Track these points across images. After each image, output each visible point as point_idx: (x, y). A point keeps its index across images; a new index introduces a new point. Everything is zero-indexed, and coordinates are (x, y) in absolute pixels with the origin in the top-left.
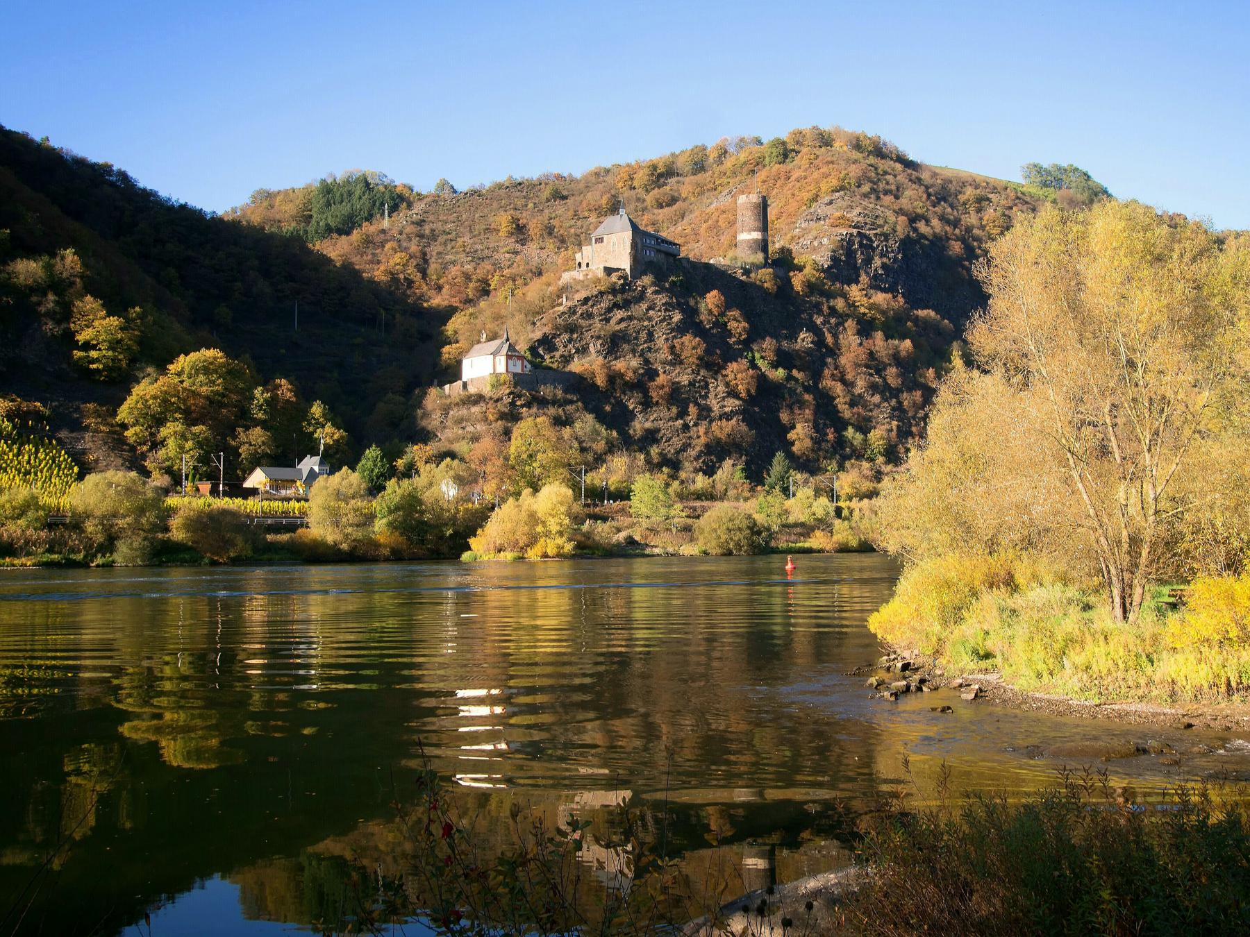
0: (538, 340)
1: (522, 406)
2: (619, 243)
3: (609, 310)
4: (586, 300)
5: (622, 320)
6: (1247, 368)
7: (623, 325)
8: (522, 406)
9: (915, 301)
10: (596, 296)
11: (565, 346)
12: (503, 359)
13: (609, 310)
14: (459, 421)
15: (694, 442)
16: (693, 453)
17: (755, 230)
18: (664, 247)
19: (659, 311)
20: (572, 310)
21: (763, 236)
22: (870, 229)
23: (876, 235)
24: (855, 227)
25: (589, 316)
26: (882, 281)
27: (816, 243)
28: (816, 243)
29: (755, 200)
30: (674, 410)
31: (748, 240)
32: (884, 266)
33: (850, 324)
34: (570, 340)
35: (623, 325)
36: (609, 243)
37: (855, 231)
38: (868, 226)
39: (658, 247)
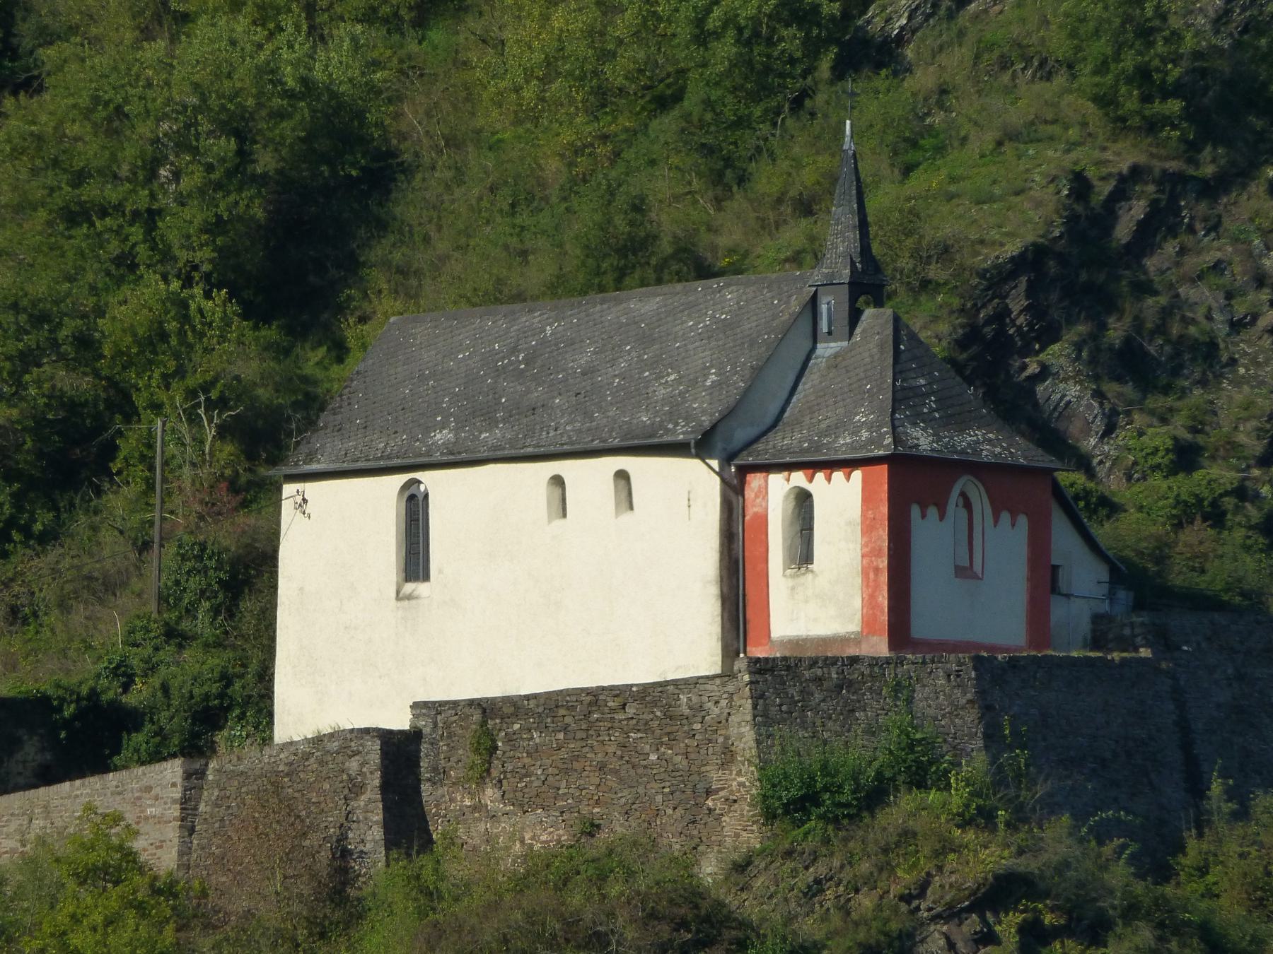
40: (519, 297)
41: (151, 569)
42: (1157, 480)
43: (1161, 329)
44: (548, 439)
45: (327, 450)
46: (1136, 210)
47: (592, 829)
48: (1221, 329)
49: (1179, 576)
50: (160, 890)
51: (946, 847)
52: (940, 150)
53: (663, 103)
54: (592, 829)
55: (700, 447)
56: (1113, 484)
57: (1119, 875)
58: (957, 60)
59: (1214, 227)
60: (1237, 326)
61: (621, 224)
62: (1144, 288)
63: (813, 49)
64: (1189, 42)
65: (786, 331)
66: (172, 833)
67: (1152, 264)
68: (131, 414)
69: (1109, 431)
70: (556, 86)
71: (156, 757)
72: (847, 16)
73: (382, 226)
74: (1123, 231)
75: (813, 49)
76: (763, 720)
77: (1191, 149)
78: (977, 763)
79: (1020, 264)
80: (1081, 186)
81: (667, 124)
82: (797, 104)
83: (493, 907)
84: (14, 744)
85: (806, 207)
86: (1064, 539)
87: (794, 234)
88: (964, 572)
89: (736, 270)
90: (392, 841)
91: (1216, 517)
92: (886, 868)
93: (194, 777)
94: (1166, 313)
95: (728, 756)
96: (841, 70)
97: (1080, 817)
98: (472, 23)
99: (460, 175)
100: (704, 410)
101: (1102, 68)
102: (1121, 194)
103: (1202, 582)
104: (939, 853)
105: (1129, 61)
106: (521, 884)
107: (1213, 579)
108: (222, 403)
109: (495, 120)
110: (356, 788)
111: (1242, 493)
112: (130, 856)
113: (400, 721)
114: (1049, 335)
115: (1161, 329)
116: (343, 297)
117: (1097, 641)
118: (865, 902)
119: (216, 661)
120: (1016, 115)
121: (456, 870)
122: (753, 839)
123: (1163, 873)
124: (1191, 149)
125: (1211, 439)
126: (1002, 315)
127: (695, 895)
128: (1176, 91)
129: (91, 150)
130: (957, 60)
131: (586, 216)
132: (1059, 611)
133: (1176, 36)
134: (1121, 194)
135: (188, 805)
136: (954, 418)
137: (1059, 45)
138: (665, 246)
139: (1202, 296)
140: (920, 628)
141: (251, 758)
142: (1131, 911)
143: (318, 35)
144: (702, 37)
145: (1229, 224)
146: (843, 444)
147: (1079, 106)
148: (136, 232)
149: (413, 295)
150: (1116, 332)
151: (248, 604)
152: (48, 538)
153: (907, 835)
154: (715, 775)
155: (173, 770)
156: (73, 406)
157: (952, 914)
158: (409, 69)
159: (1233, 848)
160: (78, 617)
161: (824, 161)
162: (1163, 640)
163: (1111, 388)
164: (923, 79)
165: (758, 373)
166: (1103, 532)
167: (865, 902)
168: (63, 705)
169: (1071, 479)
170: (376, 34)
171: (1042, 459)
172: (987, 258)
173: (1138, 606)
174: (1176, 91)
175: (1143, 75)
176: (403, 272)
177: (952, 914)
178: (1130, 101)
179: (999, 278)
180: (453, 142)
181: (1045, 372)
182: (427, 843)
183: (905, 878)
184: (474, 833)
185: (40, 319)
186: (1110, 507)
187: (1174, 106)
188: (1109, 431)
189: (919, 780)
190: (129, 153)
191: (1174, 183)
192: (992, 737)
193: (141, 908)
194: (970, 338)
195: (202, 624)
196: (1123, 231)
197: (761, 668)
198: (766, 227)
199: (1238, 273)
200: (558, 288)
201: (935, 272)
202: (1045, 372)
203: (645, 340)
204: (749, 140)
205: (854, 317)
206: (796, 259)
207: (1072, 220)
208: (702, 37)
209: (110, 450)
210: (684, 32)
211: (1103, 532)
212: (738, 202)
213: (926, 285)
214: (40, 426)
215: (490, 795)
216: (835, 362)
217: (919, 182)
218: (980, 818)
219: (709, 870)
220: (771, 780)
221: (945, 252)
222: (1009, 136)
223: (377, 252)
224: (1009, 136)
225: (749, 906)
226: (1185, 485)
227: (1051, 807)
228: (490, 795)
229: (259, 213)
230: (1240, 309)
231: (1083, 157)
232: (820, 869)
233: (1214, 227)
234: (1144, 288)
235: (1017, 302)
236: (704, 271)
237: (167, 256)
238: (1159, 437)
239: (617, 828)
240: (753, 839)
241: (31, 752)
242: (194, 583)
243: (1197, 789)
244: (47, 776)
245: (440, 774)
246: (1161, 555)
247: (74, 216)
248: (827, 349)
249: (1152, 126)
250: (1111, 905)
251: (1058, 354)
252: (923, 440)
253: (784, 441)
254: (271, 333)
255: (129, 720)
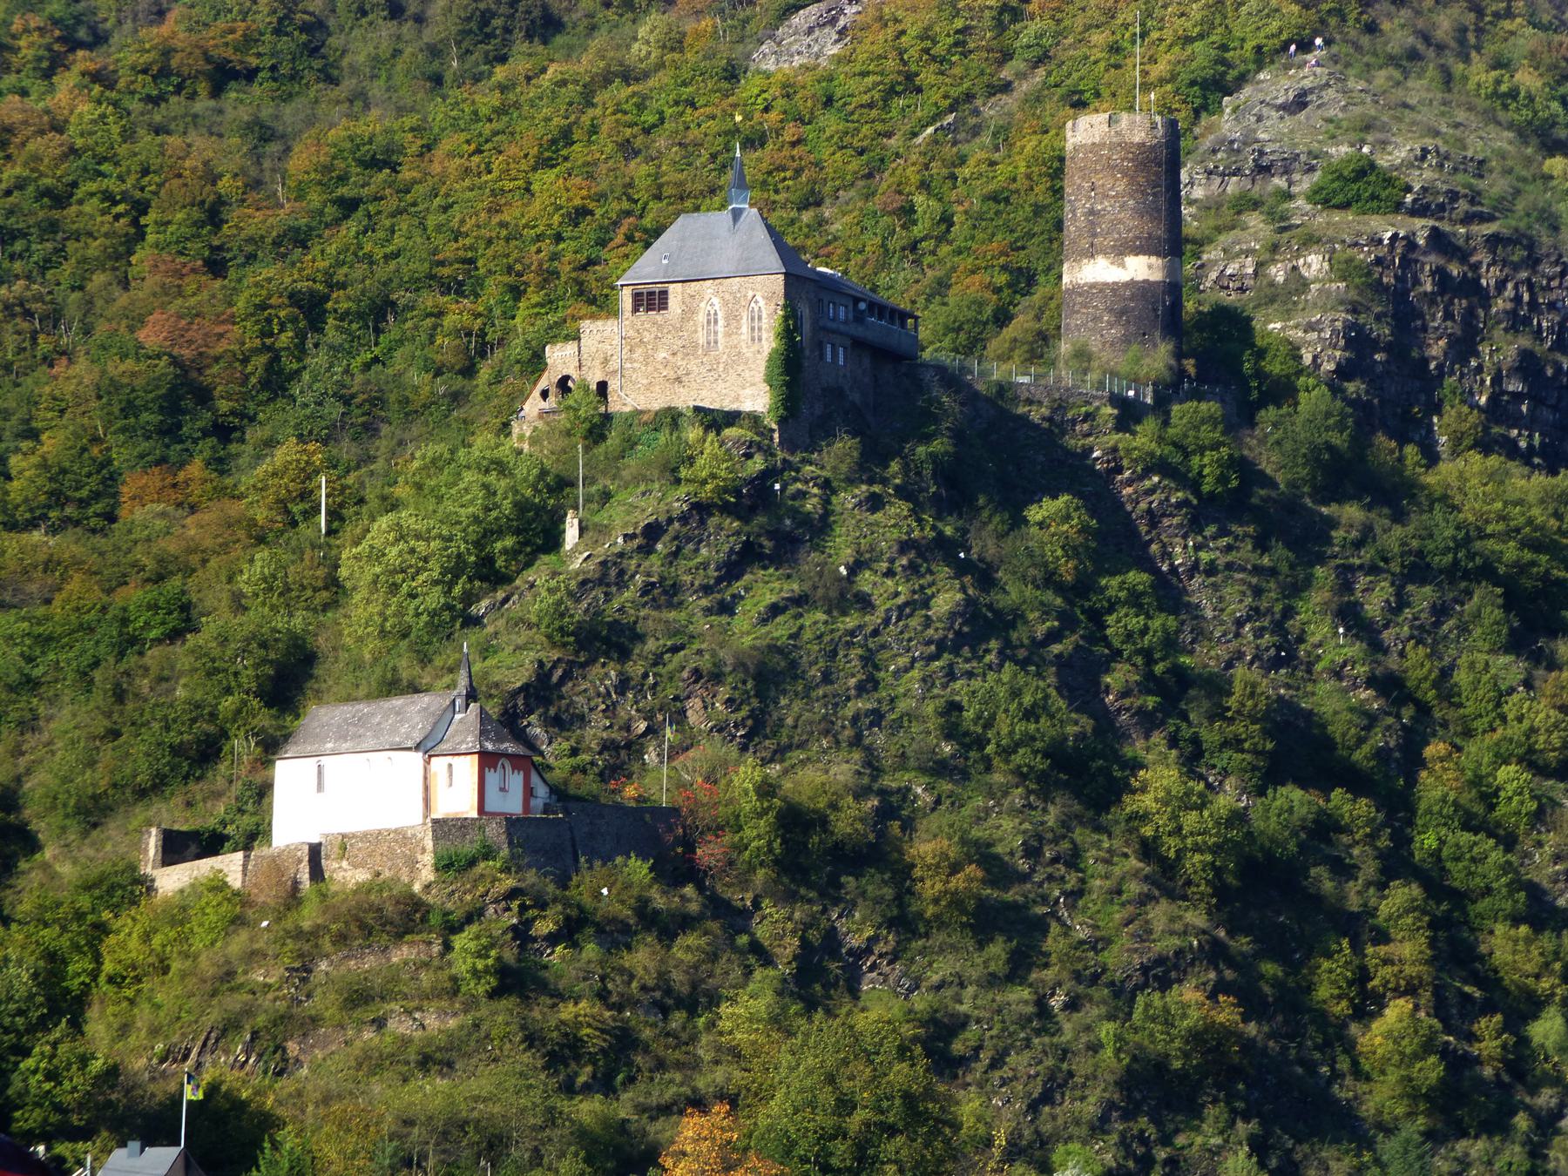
0: (525, 688)
1: (553, 939)
2: (732, 318)
3: (733, 569)
4: (653, 532)
5: (775, 610)
6: (263, 17)
7: (780, 629)
8: (553, 939)
9: (1200, 532)
10: (684, 519)
11: (610, 711)
12: (467, 768)
13: (733, 569)
14: (358, 998)
15: (1081, 1066)
16: (1090, 1108)
17: (1138, 251)
18: (875, 328)
19: (890, 573)
20: (610, 575)
21: (1173, 270)
22: (1468, 219)
23: (1494, 241)
24: (1419, 210)
25: (665, 593)
26: (1516, 421)
27: (1278, 273)
28: (1278, 273)
29: (1139, 136)
30: (998, 949)
31: (1115, 288)
32: (1528, 365)
33: (1484, 603)
34: (623, 685)
35: (780, 629)
36: (689, 313)
37: (1421, 228)
38: (1463, 206)
39: (859, 331)
40: (356, 699)
41: (233, 788)
42: (565, 760)
43: (567, 710)
44: (365, 746)
45: (291, 750)
46: (559, 672)
47: (378, 874)
48: (586, 710)
49: (572, 791)
50: (236, 894)
51: (494, 880)
52: (495, 652)
53: (405, 636)
54: (378, 874)
55: (417, 748)
56: (551, 761)
57: (551, 888)
58: (501, 623)
59: (584, 678)
60: (591, 710)
61: (389, 675)
62: (562, 697)
63: (453, 619)
64: (577, 618)
65: (445, 710)
66: (239, 876)
67: (564, 689)
68: (228, 738)
69: (550, 743)
70: (370, 629)
71: (235, 850)
72: (465, 609)
73: (311, 676)
74: (555, 679)
75: (453, 619)
76: (436, 838)
77: (577, 653)
78: (505, 852)
79: (521, 689)
80: (541, 664)
81: (404, 644)
82: (448, 637)
83: (344, 900)
84: (188, 847)
85: (451, 670)
86: (535, 779)
87: (447, 679)
88: (503, 789)
89: (426, 691)
90: (312, 878)
91: (584, 771)
92: (475, 887)
93: (247, 857)
94: (568, 705)
95: (424, 851)
96: (462, 627)
97: (539, 869)
98: (342, 611)
99: (336, 660)
100: (417, 736)
101: (548, 626)
102: (554, 667)
103: (579, 792)
104: (493, 882)
105: (557, 624)
106: (355, 892)
107: (583, 792)
108: (257, 735)
109: (348, 641)
110: (300, 861)
111: (593, 763)
112: (225, 883)
113: (315, 840)
114: (531, 712)
115: (567, 710)
116: (794, 965)
117: (545, 812)
118: (468, 897)
119: (254, 819)
120: (521, 641)
121: (334, 888)
122: (432, 877)
123: (565, 887)
124: (577, 653)
125: (583, 746)
126: (515, 706)
127: (412, 896)
128: (572, 634)
129: (216, 653)
130: (501, 623)
131: (378, 671)
132: (533, 802)
133: (572, 616)
134: (554, 667)
135: (245, 866)
136: (500, 740)
137: (534, 619)
138: (405, 683)
139: (580, 699)
140: (488, 808)
141: (265, 851)
142: (555, 900)
143: (291, 615)
144: (418, 615)
145: (590, 678)
146: (463, 748)
147: (539, 638)
148: (232, 678)
149: (320, 699)
150: (552, 712)
151: (265, 801)
152: (199, 779)
153: (482, 876)
154: (419, 857)
155: (240, 855)
156: (207, 735)
157: (496, 901)
158: (320, 625)
159: (588, 879)
160: (209, 805)
161: (457, 656)
162: (567, 812)
163: (551, 730)
164: (490, 629)
165: (435, 724)
166: (547, 776)
167: (468, 897)
168: (1442, 1020)
169: (537, 759)
170: (310, 614)
171: (529, 753)
172: (511, 687)
173: (559, 800)
174: (572, 634)
175: (561, 629)
176: (318, 691)
177: (496, 901)
178: (557, 638)
179: (514, 694)
180: (334, 649)
181: (529, 724)
182: (323, 879)
183: (481, 889)
184: (339, 876)
185: (198, 707)
186: (550, 768)
187: (572, 639)
188: (550, 743)
189: (486, 857)
190: (229, 653)
191: (571, 664)
192: (510, 843)
193: (229, 900)
194: (505, 713)
195: (250, 807)
196: (555, 679)
197: (435, 822)
198: (438, 677)
199: (591, 692)
200: (369, 697)
201: (493, 691)
202: (529, 724)
203: (398, 713)
204: (431, 649)
205: (467, 706)
206: (448, 687)
207: (538, 675)
208: (418, 615)
209: (220, 750)
210: (411, 612)
211: (547, 776)
212: (429, 668)
213: (491, 696)
214: (199, 742)
215: (345, 864)
216: (461, 721)
217: (488, 663)
218: (506, 870)
219: (417, 888)
220: (438, 858)
221: (497, 685)
222: (518, 648)
223: (309, 685)
224: (518, 648)
225: (430, 899)
226: (573, 761)
227: (529, 866)
228: (345, 864)
229: (271, 672)
230: (592, 704)
231: (542, 655)
232: (453, 887)
233: (584, 678)
234: (562, 697)
235: (520, 702)
236: (417, 691)
237: (239, 686)
238: (566, 745)
239: (387, 874)
240: (432, 877)
241: (193, 849)
242: (248, 793)
243: (576, 860)
244: (199, 857)
245: (328, 857)
246: (566, 782)
247: (209, 674)
248: (458, 717)
249: (564, 645)
250: (548, 898)
251: (533, 718)
252: (489, 746)
253: (443, 747)
254: (273, 711)
255: (227, 838)
